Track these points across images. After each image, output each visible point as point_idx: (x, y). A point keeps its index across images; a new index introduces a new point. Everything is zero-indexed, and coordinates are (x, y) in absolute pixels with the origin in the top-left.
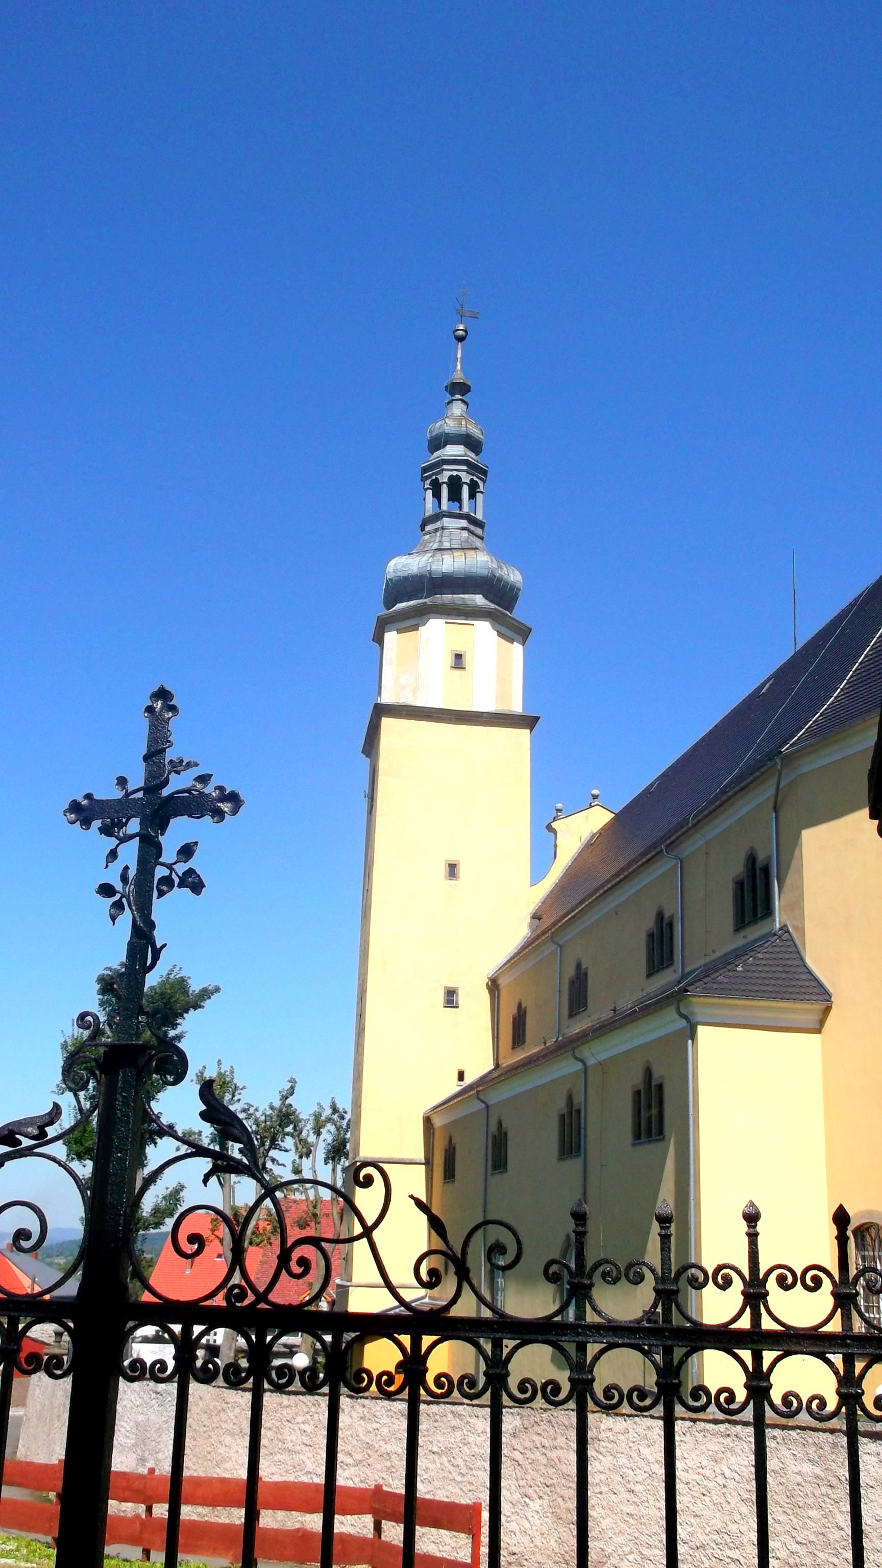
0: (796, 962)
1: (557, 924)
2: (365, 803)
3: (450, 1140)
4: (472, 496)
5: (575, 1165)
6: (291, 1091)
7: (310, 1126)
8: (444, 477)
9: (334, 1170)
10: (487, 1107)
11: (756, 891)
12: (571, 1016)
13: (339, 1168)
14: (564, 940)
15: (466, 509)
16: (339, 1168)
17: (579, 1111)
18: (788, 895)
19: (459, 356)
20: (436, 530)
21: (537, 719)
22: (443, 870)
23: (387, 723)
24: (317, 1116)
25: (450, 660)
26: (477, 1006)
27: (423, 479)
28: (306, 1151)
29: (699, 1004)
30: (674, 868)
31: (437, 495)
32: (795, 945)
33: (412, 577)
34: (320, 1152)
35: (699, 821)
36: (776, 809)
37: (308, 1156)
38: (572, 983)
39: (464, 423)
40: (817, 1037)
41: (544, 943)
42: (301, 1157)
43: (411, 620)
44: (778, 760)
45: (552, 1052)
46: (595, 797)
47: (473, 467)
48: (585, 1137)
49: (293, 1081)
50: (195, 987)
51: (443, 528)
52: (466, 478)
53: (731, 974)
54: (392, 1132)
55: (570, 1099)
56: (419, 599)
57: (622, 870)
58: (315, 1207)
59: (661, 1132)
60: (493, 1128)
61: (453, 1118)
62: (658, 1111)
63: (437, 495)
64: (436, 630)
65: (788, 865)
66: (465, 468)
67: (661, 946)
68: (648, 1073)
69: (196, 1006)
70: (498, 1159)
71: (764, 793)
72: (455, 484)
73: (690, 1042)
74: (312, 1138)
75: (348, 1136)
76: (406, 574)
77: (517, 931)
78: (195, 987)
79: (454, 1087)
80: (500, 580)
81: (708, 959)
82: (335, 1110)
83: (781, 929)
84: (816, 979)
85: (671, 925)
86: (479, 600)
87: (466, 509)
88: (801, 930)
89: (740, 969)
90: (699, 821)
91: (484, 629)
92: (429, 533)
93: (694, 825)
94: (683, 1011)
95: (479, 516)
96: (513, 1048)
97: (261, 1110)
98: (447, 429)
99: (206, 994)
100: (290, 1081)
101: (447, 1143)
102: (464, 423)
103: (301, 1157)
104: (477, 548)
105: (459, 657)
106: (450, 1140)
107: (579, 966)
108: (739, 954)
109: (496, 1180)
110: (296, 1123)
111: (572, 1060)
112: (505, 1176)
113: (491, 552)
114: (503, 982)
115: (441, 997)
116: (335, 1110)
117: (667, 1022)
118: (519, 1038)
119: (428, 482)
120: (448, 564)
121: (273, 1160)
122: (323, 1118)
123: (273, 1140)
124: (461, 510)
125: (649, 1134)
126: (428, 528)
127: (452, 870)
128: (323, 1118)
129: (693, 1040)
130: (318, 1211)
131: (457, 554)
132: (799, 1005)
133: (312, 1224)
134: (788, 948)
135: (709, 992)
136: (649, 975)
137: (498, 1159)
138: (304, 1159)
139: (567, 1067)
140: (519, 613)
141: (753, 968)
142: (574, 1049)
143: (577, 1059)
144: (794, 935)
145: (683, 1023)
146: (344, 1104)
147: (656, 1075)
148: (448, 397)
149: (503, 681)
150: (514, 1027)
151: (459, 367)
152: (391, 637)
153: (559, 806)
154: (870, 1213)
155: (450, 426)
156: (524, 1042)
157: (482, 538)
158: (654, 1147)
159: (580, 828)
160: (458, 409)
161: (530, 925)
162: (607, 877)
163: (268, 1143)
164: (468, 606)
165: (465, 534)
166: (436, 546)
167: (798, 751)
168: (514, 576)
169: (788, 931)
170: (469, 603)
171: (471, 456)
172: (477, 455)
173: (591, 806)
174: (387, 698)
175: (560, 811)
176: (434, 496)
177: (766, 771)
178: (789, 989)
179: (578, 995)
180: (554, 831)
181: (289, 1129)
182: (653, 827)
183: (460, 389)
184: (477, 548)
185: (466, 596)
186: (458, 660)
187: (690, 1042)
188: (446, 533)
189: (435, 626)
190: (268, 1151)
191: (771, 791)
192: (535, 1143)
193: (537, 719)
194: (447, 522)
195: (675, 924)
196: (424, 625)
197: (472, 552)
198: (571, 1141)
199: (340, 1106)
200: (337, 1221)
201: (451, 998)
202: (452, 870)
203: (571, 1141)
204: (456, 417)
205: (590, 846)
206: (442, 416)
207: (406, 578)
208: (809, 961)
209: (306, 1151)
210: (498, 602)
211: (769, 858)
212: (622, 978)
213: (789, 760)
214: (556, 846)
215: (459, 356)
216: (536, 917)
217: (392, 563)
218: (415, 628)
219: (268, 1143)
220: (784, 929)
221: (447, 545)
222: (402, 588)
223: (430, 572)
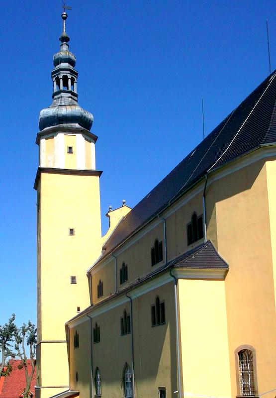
0: (215, 254)
1: (116, 247)
2: (36, 208)
3: (76, 332)
4: (72, 84)
5: (128, 337)
6: (13, 319)
7: (21, 331)
8: (61, 76)
9: (31, 347)
11: (196, 229)
12: (121, 283)
13: (33, 346)
14: (118, 255)
15: (70, 89)
16: (33, 346)
17: (129, 317)
18: (210, 228)
19: (64, 26)
20: (59, 98)
21: (101, 172)
23: (43, 175)
24: (23, 328)
25: (67, 150)
27: (52, 77)
28: (20, 341)
29: (178, 271)
30: (162, 223)
31: (58, 84)
32: (214, 248)
33: (50, 117)
34: (25, 341)
35: (173, 203)
36: (204, 196)
37: (21, 342)
38: (121, 271)
39: (68, 53)
40: (223, 282)
41: (110, 256)
42: (18, 343)
43: (51, 134)
44: (206, 176)
45: (114, 297)
46: (124, 203)
47: (72, 72)
48: (132, 323)
49: (14, 315)
51: (61, 97)
52: (69, 76)
53: (190, 259)
54: (54, 330)
55: (125, 312)
56: (53, 126)
57: (140, 227)
58: (24, 361)
60: (94, 326)
61: (75, 326)
62: (163, 313)
63: (58, 84)
64: (62, 140)
65: (210, 218)
66: (69, 72)
67: (157, 254)
68: (158, 299)
70: (96, 336)
71: (200, 189)
72: (65, 79)
73: (175, 286)
74: (22, 336)
75: (36, 334)
76: (47, 116)
77: (97, 254)
79: (76, 313)
80: (85, 117)
81: (177, 256)
82: (30, 325)
83: (207, 242)
84: (222, 260)
86: (77, 125)
87: (70, 89)
88: (216, 242)
89: (193, 257)
90: (173, 203)
91: (79, 137)
92: (56, 99)
93: (170, 205)
94: (172, 274)
95: (75, 92)
96: (98, 298)
97: (2, 327)
98: (61, 56)
100: (13, 315)
101: (75, 334)
102: (68, 53)
103: (18, 343)
104: (75, 105)
105: (70, 148)
106: (76, 332)
107: (124, 264)
108: (190, 253)
109: (96, 345)
110: (15, 330)
111: (126, 297)
112: (100, 343)
113: (81, 106)
114: (92, 273)
115: (69, 280)
116: (30, 325)
117: (167, 279)
118: (100, 293)
119: (55, 78)
120: (64, 111)
121: (8, 345)
122: (26, 328)
123: (8, 337)
124: (68, 89)
126: (56, 97)
127: (72, 232)
128: (26, 328)
129: (176, 285)
130: (26, 362)
131: (67, 107)
132: (216, 270)
133: (24, 367)
135: (183, 266)
136: (152, 265)
137: (96, 336)
138: (19, 344)
139: (124, 300)
140: (93, 130)
141: (198, 257)
142: (127, 293)
144: (213, 244)
145: (173, 278)
146: (34, 322)
147: (161, 300)
148: (61, 43)
149: (88, 158)
151: (64, 30)
152: (43, 142)
153: (111, 206)
154: (245, 346)
155: (62, 55)
156: (102, 295)
157: (77, 101)
158: (162, 327)
159: (119, 215)
160: (65, 48)
161: (102, 252)
162: (130, 233)
163: (5, 339)
164: (73, 128)
165: (70, 99)
166: (59, 104)
167: (214, 171)
168: (90, 116)
169: (210, 243)
170: (73, 127)
171: (71, 67)
172: (73, 67)
173: (123, 206)
174: (43, 165)
175: (111, 208)
176: (57, 84)
177: (201, 180)
178: (212, 264)
179: (124, 274)
180: (109, 217)
181: (13, 333)
182: (148, 211)
183: (65, 39)
184: (75, 105)
185: (72, 124)
187: (175, 286)
188: (63, 99)
189: (61, 136)
190: (6, 341)
191: (204, 188)
192: (111, 330)
193: (101, 172)
194: (63, 94)
195: (163, 244)
196: (56, 136)
197: (74, 106)
198: (126, 326)
199: (32, 324)
200: (33, 366)
201: (73, 280)
202: (72, 232)
203: (126, 326)
204: (64, 51)
205: (123, 221)
206: (59, 51)
207: (47, 118)
208: (219, 253)
209: (20, 341)
210: (85, 126)
211: (202, 215)
212: (141, 266)
213: (210, 175)
214: (110, 222)
215: (64, 26)
216: (104, 249)
217: (42, 112)
218: (53, 137)
219: (5, 339)
220: (209, 242)
221: (63, 104)
223: (58, 115)
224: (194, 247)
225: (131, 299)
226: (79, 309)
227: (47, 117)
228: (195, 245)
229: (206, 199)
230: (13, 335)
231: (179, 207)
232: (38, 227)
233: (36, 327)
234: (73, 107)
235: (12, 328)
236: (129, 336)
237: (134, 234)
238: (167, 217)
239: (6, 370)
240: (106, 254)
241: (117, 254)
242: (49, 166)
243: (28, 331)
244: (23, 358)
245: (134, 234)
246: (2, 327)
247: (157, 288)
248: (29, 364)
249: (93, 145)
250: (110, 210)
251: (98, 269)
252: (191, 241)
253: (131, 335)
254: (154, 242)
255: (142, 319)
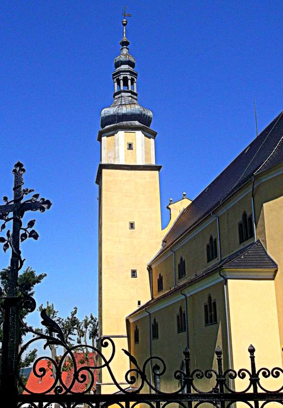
1: (172, 244)
4: (132, 84)
6: (75, 312)
8: (121, 77)
9: (93, 341)
10: (150, 314)
11: (247, 227)
13: (95, 340)
15: (130, 89)
16: (95, 340)
17: (184, 314)
18: (259, 228)
19: (124, 31)
20: (119, 97)
22: (128, 226)
23: (104, 171)
24: (86, 321)
25: (127, 146)
26: (143, 275)
27: (113, 79)
28: (82, 334)
29: (227, 271)
31: (119, 84)
34: (88, 335)
37: (83, 336)
38: (179, 266)
42: (80, 337)
43: (112, 132)
44: (253, 178)
45: (173, 293)
46: (184, 195)
47: (132, 73)
49: (76, 308)
50: (37, 274)
51: (122, 97)
52: (129, 77)
53: (239, 259)
54: (114, 325)
56: (113, 124)
59: (216, 320)
61: (134, 321)
62: (215, 312)
63: (119, 84)
66: (129, 73)
68: (210, 298)
69: (38, 282)
74: (84, 330)
75: (98, 328)
77: (159, 248)
78: (37, 274)
79: (136, 308)
80: (144, 115)
81: (230, 254)
82: (92, 318)
83: (257, 241)
84: (271, 260)
85: (215, 242)
86: (137, 123)
87: (130, 89)
88: (265, 241)
91: (139, 134)
92: (116, 98)
94: (183, 293)
95: (135, 91)
96: (158, 292)
97: (64, 320)
99: (41, 277)
103: (80, 337)
104: (134, 104)
108: (241, 251)
109: (154, 341)
113: (140, 105)
114: (153, 267)
115: (130, 274)
116: (92, 318)
117: (217, 279)
118: (160, 288)
120: (124, 110)
121: (70, 338)
122: (88, 322)
123: (70, 331)
124: (128, 89)
125: (211, 321)
126: (116, 97)
127: (132, 226)
131: (127, 106)
133: (86, 362)
134: (261, 249)
136: (208, 262)
140: (151, 128)
142: (181, 291)
143: (183, 294)
145: (222, 279)
146: (96, 316)
148: (121, 47)
149: (147, 153)
150: (158, 283)
152: (104, 139)
153: (171, 199)
155: (123, 58)
156: (162, 289)
158: (214, 326)
159: (179, 207)
160: (125, 51)
161: (162, 245)
163: (67, 332)
165: (130, 98)
166: (119, 103)
167: (260, 174)
168: (150, 114)
169: (260, 242)
170: (133, 124)
172: (133, 68)
174: (104, 161)
175: (171, 201)
178: (259, 264)
179: (182, 271)
180: (170, 209)
181: (75, 326)
182: (206, 206)
183: (125, 44)
184: (134, 104)
186: (130, 146)
188: (123, 98)
189: (121, 134)
190: (68, 335)
191: (251, 189)
192: (168, 327)
194: (123, 94)
197: (133, 105)
198: (182, 326)
199: (94, 317)
201: (134, 274)
202: (132, 226)
203: (182, 326)
205: (183, 214)
206: (119, 54)
208: (268, 253)
209: (82, 334)
210: (144, 124)
211: (251, 215)
212: (198, 264)
213: (257, 177)
214: (170, 214)
216: (164, 241)
218: (113, 135)
219: (67, 332)
220: (258, 241)
221: (123, 103)
222: (107, 120)
224: (246, 245)
225: (185, 296)
226: (139, 303)
227: (109, 116)
228: (247, 243)
229: (255, 199)
230: (75, 328)
231: (231, 205)
232: (99, 222)
233: (97, 321)
234: (133, 106)
235: (74, 322)
236: (185, 334)
237: (197, 225)
238: (220, 214)
239: (68, 364)
240: (166, 247)
241: (176, 249)
242: (110, 162)
243: (91, 325)
244: (85, 352)
245: (197, 225)
246: (64, 320)
247: (218, 283)
248: (91, 358)
249: (152, 141)
250: (171, 202)
251: (158, 263)
252: (242, 240)
253: (186, 332)
254: (209, 238)
255: (196, 317)
